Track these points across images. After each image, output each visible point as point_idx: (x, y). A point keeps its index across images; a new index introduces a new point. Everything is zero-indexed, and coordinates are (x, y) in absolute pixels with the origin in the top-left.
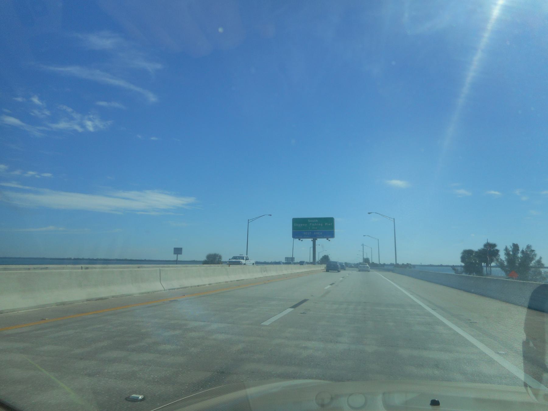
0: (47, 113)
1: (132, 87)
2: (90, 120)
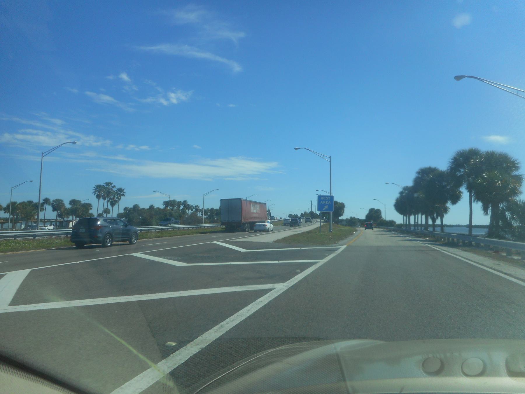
0: (135, 88)
1: (218, 59)
2: (173, 92)
